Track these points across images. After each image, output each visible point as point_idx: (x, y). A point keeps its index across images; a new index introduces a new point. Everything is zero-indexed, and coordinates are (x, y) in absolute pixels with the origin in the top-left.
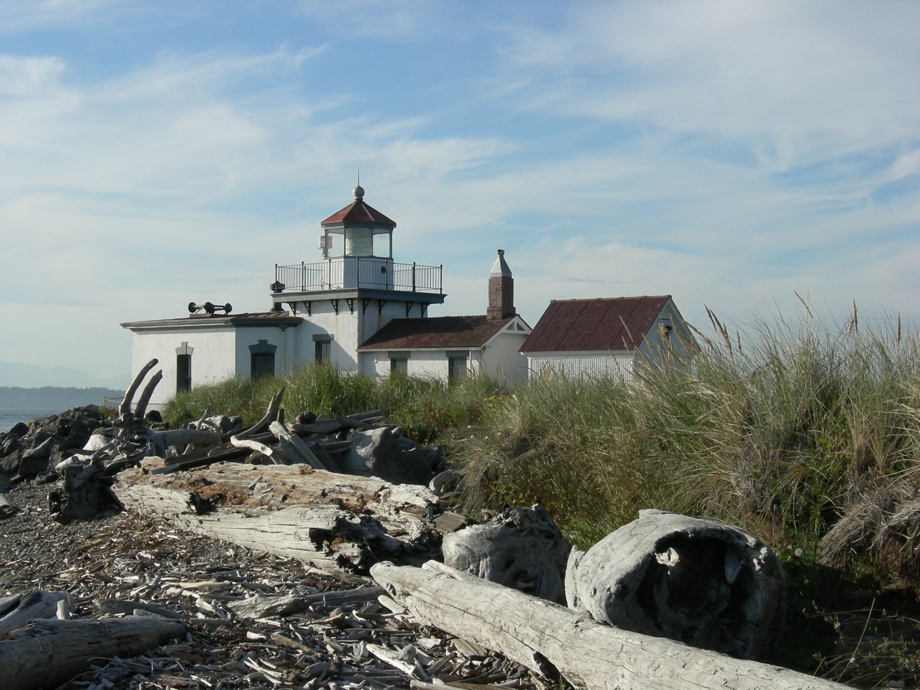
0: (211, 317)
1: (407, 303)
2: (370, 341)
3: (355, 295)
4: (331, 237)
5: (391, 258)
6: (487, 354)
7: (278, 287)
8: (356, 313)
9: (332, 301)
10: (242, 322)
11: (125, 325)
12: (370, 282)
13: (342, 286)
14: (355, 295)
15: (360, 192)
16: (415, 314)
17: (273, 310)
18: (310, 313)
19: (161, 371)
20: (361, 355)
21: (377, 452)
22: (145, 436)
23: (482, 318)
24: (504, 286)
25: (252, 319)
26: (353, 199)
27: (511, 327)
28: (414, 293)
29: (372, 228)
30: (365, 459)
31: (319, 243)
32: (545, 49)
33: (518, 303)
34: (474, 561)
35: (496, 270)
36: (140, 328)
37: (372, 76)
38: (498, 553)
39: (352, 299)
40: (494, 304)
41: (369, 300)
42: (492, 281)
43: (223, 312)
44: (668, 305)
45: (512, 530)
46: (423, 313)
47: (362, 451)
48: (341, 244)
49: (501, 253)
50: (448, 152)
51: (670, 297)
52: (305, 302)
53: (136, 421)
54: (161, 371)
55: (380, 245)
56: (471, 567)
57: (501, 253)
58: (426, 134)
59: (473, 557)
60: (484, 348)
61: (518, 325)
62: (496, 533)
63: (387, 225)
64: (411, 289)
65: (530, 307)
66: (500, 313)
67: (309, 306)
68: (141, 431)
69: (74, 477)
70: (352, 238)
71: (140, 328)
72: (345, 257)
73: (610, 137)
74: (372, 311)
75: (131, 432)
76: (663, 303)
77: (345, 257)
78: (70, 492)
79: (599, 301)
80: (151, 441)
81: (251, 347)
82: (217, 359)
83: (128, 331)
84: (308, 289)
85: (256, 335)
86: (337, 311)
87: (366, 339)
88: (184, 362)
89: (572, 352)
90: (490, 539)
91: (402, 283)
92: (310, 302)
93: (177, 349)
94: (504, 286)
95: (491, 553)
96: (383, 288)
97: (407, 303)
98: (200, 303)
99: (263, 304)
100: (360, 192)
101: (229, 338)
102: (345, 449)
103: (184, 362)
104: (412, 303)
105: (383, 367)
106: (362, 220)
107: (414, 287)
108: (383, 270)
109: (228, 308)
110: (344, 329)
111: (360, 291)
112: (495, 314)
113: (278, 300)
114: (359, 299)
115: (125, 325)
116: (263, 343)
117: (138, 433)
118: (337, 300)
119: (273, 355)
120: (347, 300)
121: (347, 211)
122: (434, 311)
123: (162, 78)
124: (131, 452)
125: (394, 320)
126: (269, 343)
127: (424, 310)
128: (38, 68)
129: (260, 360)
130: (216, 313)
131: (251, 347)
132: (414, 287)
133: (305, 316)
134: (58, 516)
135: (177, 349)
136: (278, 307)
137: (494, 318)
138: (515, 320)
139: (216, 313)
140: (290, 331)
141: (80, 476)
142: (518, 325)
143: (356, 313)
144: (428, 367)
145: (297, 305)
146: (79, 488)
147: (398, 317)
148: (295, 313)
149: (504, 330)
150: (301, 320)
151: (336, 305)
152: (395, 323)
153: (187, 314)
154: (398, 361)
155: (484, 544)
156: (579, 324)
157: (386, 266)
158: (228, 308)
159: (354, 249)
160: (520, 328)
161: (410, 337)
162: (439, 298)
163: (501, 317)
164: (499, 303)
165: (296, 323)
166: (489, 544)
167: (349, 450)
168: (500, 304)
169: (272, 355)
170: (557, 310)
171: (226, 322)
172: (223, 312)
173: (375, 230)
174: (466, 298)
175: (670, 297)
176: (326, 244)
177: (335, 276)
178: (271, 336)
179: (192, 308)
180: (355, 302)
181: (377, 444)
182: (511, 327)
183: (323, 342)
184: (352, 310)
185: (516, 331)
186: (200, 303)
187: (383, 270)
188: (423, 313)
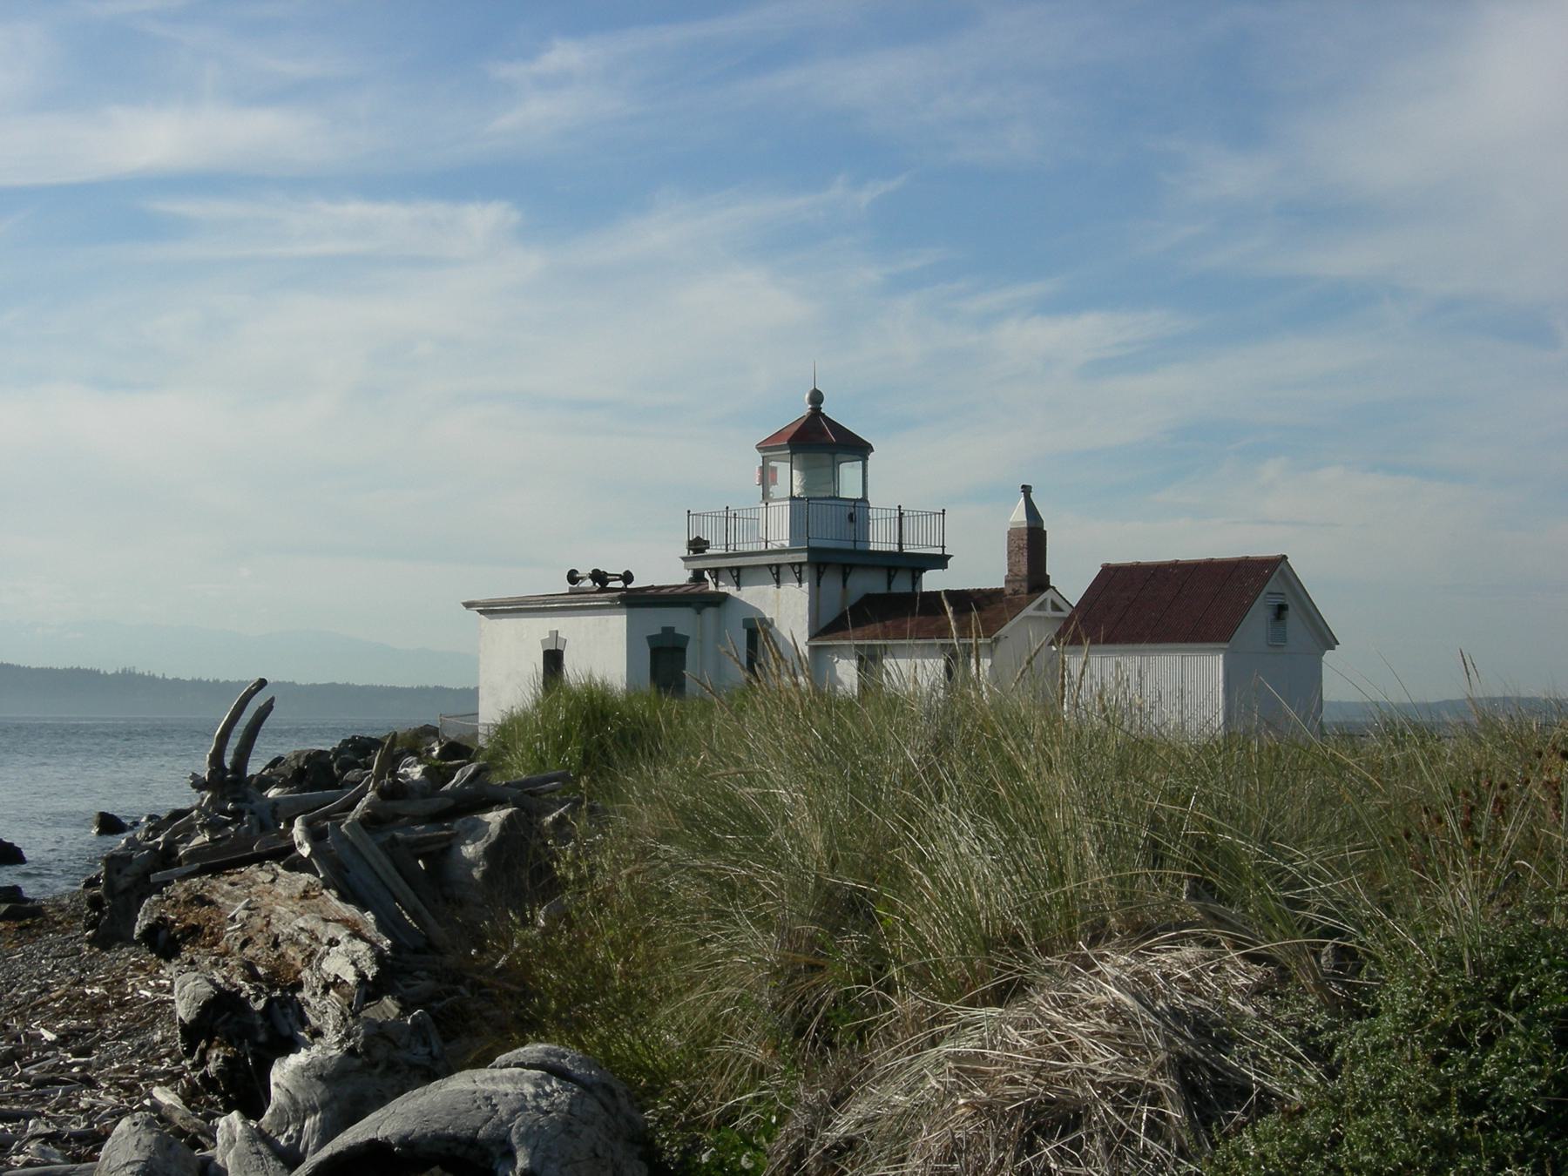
0: (599, 591)
1: (889, 569)
2: (826, 628)
3: (803, 557)
4: (774, 469)
5: (864, 499)
6: (998, 652)
7: (698, 546)
8: (806, 585)
9: (770, 566)
10: (636, 600)
11: (468, 605)
12: (830, 536)
13: (787, 544)
14: (803, 557)
15: (816, 398)
16: (901, 585)
17: (691, 580)
18: (738, 585)
19: (272, 699)
20: (813, 649)
21: (492, 852)
22: (242, 805)
23: (997, 593)
24: (1032, 542)
25: (651, 596)
26: (805, 409)
27: (1041, 607)
28: (900, 554)
29: (834, 454)
30: (472, 864)
31: (758, 474)
32: (1234, 176)
33: (1051, 569)
34: (296, 1119)
35: (1019, 516)
36: (491, 609)
37: (973, 222)
38: (335, 1106)
39: (800, 564)
40: (1016, 569)
41: (826, 565)
42: (1013, 534)
43: (620, 584)
44: (1282, 573)
45: (358, 1062)
46: (914, 584)
47: (469, 850)
48: (789, 478)
49: (1026, 490)
50: (1088, 332)
51: (1285, 557)
52: (731, 569)
53: (231, 781)
54: (272, 699)
55: (849, 480)
56: (290, 1131)
57: (1026, 490)
58: (1055, 307)
59: (296, 1111)
60: (997, 640)
61: (1053, 602)
62: (330, 1067)
63: (858, 449)
64: (896, 548)
65: (1071, 577)
66: (1025, 584)
67: (738, 575)
68: (239, 796)
69: (119, 871)
70: (802, 469)
71: (491, 609)
72: (792, 498)
73: (1331, 306)
74: (832, 583)
75: (223, 798)
76: (1276, 566)
77: (792, 498)
78: (113, 897)
79: (1176, 565)
80: (252, 813)
81: (651, 639)
82: (602, 652)
83: (473, 612)
84: (741, 548)
85: (657, 620)
86: (778, 582)
87: (828, 618)
88: (553, 660)
89: (1130, 647)
90: (320, 1077)
91: (881, 539)
92: (739, 569)
93: (543, 642)
94: (1032, 542)
95: (324, 1106)
96: (850, 546)
97: (889, 569)
98: (584, 570)
99: (676, 574)
100: (816, 398)
101: (616, 624)
102: (444, 845)
103: (553, 660)
104: (897, 569)
105: (846, 672)
106: (819, 440)
107: (900, 544)
108: (851, 518)
109: (628, 577)
110: (788, 608)
111: (811, 551)
112: (1017, 586)
113: (699, 565)
114: (809, 563)
115: (468, 605)
116: (668, 631)
117: (234, 801)
118: (778, 566)
119: (683, 650)
120: (792, 565)
121: (796, 428)
122: (932, 581)
123: (659, 232)
124: (218, 831)
125: (1108, 571)
126: (677, 631)
127: (916, 580)
128: (484, 218)
129: (664, 660)
130: (610, 585)
131: (651, 639)
132: (900, 544)
133: (730, 590)
134: (94, 935)
135: (543, 642)
136: (698, 576)
137: (1015, 592)
138: (1048, 595)
139: (610, 585)
140: (710, 612)
141: (129, 870)
142: (1053, 602)
143: (806, 585)
144: (915, 671)
145: (721, 574)
146: (125, 891)
147: (876, 592)
148: (716, 585)
149: (1029, 610)
150: (726, 596)
151: (776, 574)
152: (869, 600)
153: (565, 587)
154: (868, 661)
155: (312, 1086)
156: (1151, 604)
157: (857, 512)
158: (628, 577)
159: (806, 486)
160: (1056, 608)
161: (888, 623)
162: (940, 561)
163: (1025, 590)
164: (1024, 569)
165: (720, 600)
166: (320, 1088)
167: (450, 847)
168: (1024, 570)
169: (681, 650)
170: (1113, 580)
171: (612, 600)
172: (620, 584)
173: (838, 457)
174: (978, 563)
175: (1285, 557)
176: (766, 477)
177: (776, 529)
178: (681, 620)
179: (573, 577)
180: (805, 568)
181: (493, 838)
182: (1041, 607)
183: (757, 632)
184: (800, 581)
185: (1049, 612)
186: (584, 570)
187: (851, 518)
188: (914, 584)
